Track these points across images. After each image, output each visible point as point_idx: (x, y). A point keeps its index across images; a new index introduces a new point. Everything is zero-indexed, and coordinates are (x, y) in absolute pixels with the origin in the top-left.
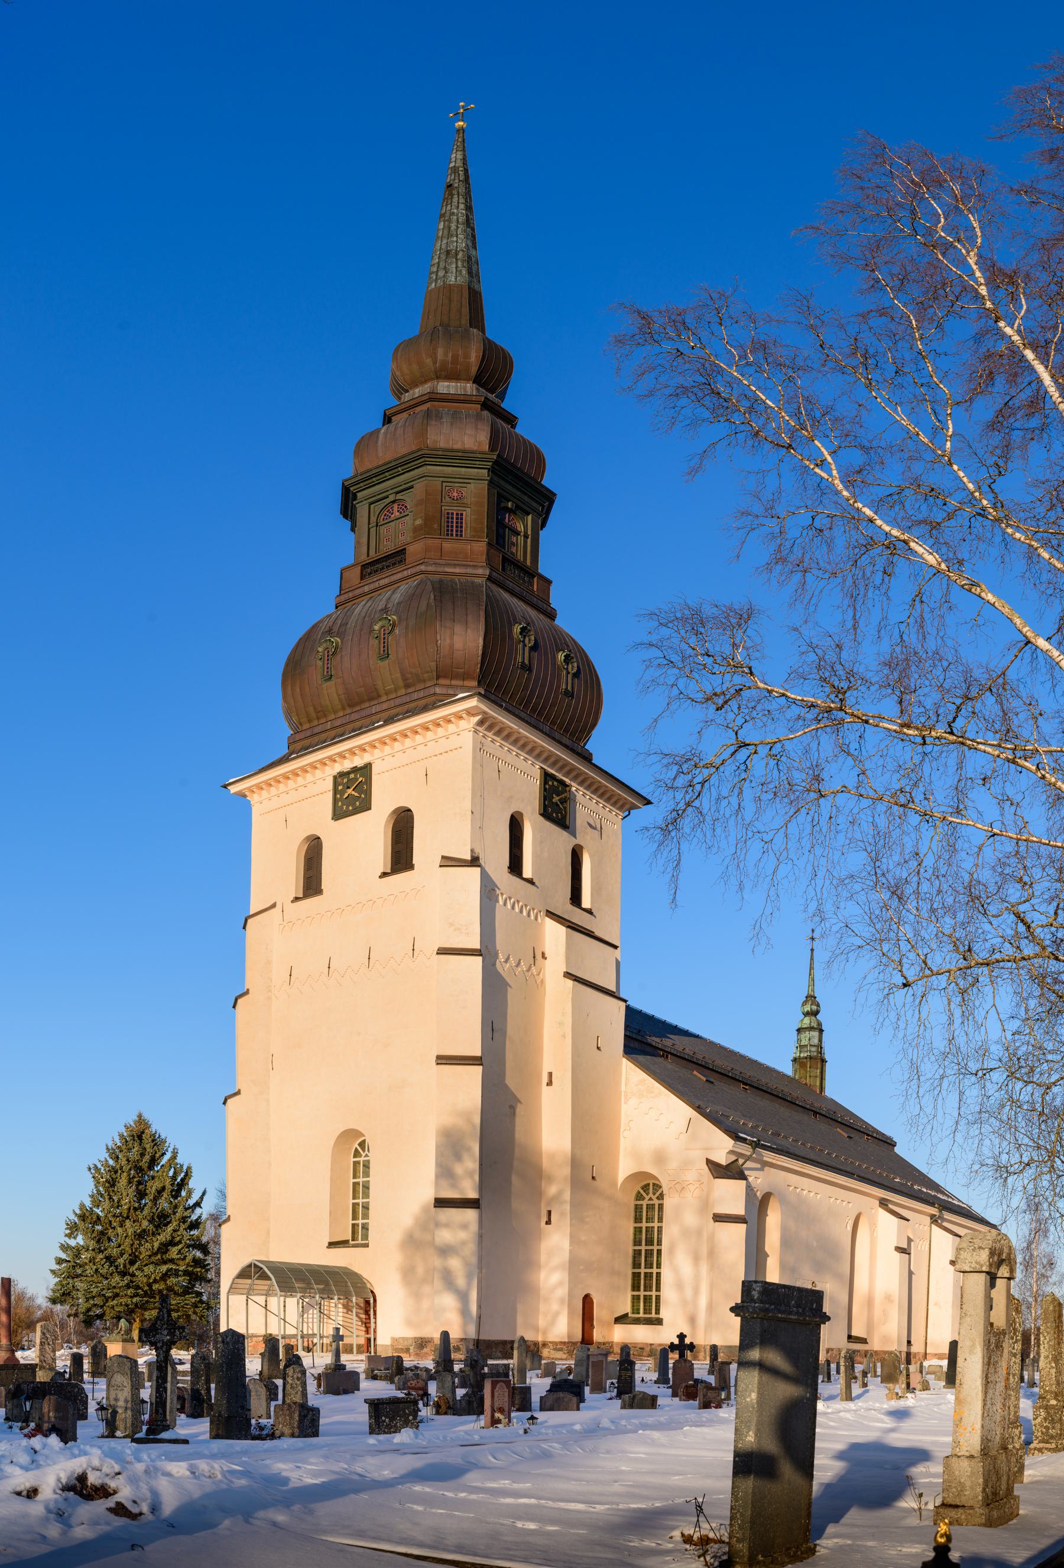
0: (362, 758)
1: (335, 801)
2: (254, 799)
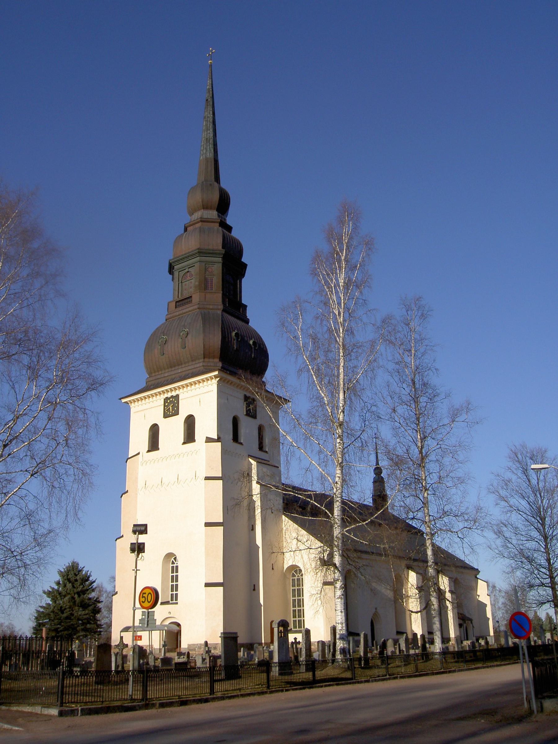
0: (175, 392)
1: (164, 409)
2: (132, 405)
